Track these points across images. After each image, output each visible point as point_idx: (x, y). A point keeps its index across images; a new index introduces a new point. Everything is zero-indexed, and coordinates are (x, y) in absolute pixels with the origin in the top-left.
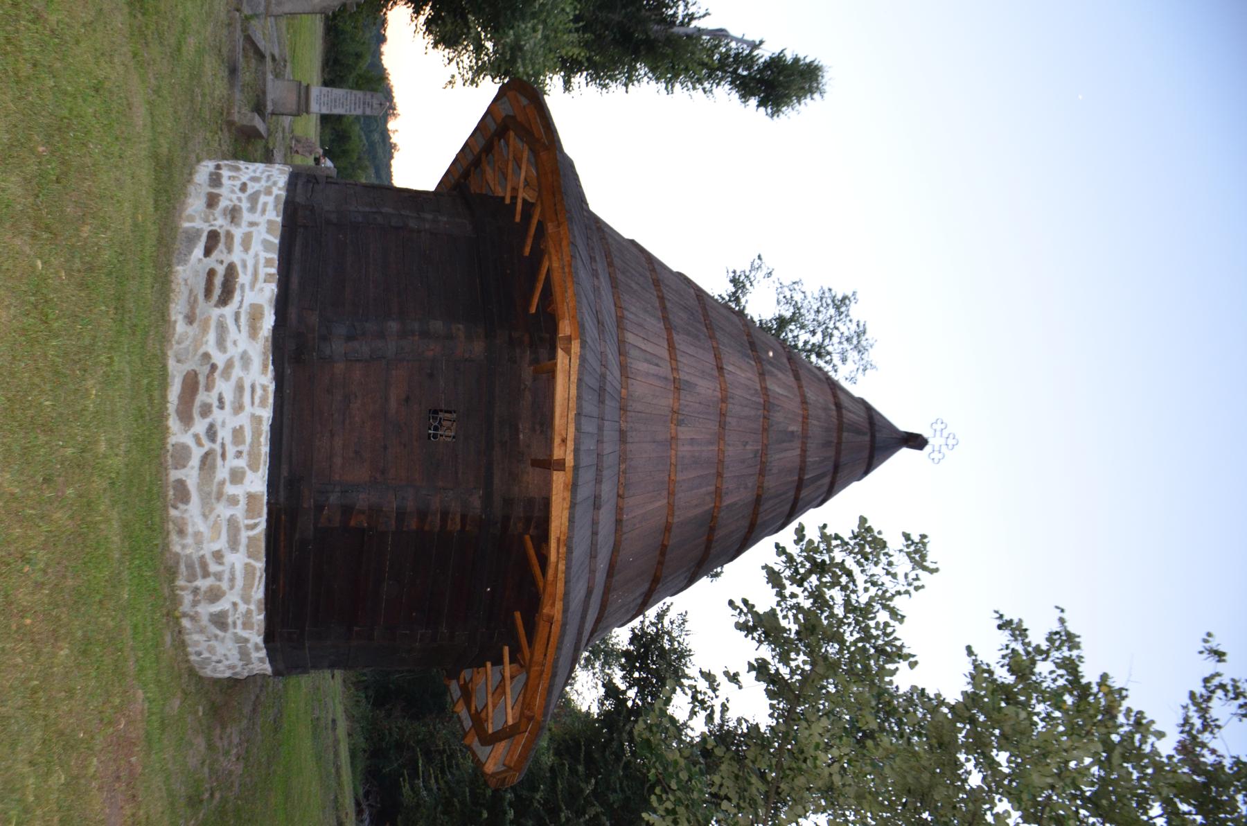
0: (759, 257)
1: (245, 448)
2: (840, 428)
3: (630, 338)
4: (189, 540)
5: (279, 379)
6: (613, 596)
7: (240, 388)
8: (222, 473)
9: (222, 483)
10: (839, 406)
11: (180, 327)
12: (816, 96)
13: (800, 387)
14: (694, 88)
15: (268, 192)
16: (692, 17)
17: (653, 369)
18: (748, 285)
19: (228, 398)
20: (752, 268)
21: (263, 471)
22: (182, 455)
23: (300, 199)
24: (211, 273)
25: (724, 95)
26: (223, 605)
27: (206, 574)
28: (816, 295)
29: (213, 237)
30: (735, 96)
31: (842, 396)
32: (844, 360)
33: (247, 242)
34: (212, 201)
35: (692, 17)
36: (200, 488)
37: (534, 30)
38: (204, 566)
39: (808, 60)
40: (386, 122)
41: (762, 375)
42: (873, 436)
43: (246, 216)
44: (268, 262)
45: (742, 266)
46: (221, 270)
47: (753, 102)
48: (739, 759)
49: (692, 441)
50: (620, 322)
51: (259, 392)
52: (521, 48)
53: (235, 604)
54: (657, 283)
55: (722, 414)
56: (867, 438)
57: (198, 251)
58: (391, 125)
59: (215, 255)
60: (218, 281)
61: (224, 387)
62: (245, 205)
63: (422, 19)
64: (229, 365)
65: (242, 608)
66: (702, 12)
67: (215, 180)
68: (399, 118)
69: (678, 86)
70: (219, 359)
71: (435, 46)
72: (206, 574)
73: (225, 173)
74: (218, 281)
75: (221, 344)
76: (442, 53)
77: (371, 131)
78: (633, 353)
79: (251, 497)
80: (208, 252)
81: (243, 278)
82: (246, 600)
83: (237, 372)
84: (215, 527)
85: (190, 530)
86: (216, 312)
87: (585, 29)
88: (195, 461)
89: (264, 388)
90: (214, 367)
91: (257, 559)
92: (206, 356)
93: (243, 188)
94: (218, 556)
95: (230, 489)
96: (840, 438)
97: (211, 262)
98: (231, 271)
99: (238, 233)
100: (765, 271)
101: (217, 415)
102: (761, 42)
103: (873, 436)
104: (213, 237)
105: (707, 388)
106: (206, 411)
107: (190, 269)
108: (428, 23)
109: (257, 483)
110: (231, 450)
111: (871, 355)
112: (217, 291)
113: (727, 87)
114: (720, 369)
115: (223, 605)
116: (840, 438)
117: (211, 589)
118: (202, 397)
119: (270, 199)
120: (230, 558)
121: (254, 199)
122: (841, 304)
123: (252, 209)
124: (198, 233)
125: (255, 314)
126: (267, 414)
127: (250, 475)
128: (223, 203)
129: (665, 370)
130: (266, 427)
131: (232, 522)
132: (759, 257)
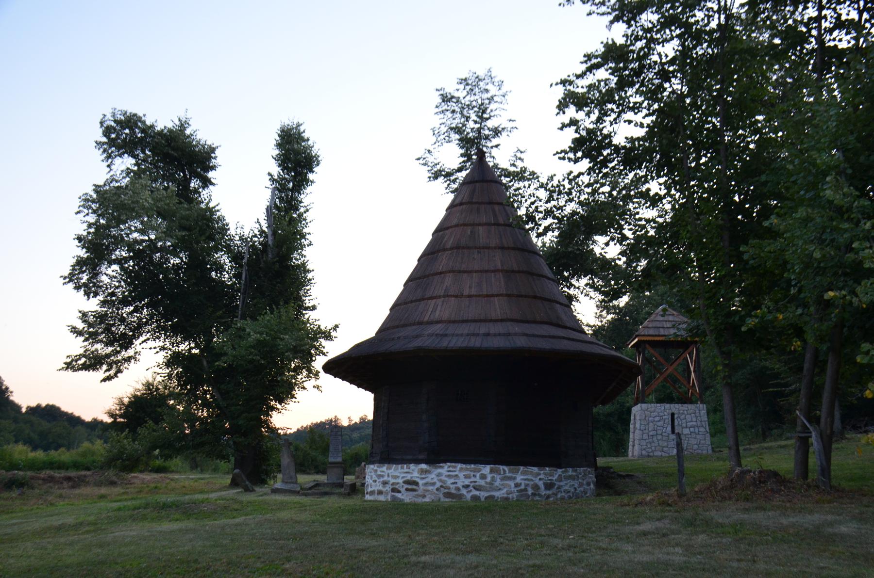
0: (418, 159)
1: (472, 474)
2: (470, 203)
3: (426, 319)
4: (510, 496)
5: (445, 462)
6: (538, 319)
7: (449, 476)
8: (482, 483)
9: (486, 483)
10: (461, 204)
11: (427, 500)
12: (302, 129)
13: (451, 227)
14: (305, 220)
15: (376, 471)
16: (262, 232)
17: (439, 308)
18: (438, 167)
19: (452, 481)
20: (425, 164)
21: (481, 466)
22: (475, 498)
23: (378, 458)
24: (407, 490)
25: (309, 197)
26: (541, 484)
27: (525, 490)
28: (442, 116)
29: (393, 490)
30: (309, 189)
31: (457, 201)
32: (487, 91)
33: (396, 477)
34: (380, 493)
35: (262, 232)
36: (489, 491)
37: (282, 340)
38: (521, 491)
39: (278, 138)
40: (343, 427)
41: (445, 250)
42: (477, 182)
43: (386, 478)
44: (402, 468)
45: (425, 173)
46: (406, 486)
47: (311, 176)
48: (679, 220)
49: (470, 287)
50: (420, 323)
51: (451, 469)
52: (295, 347)
53: (540, 479)
54: (433, 253)
55: (460, 272)
56: (478, 185)
57: (399, 495)
58: (345, 423)
59: (400, 489)
60: (410, 487)
61: (449, 482)
62: (382, 480)
63: (279, 406)
64: (441, 481)
65: (542, 476)
66: (257, 226)
67: (372, 493)
68: (339, 417)
69: (305, 230)
70: (438, 484)
71: (293, 397)
72: (525, 490)
73: (370, 489)
74: (410, 487)
75: (433, 484)
76: (298, 393)
77: (351, 440)
78: (432, 318)
79: (491, 471)
80: (399, 492)
81: (409, 477)
82: (539, 474)
83: (443, 478)
84: (504, 486)
85: (505, 495)
86: (421, 487)
87: (277, 305)
88: (477, 493)
89: (449, 467)
90: (441, 486)
91: (519, 470)
92: (437, 489)
93: (375, 481)
94: (517, 485)
95: (489, 479)
96: (476, 203)
97: (403, 490)
98: (407, 482)
99: (392, 481)
100: (427, 155)
101: (460, 485)
102: (269, 174)
103: (477, 182)
104: (393, 490)
105: (449, 280)
106: (458, 489)
107: (406, 497)
108: (281, 402)
109: (486, 469)
110: (473, 479)
111: (482, 73)
112: (414, 487)
113: (302, 196)
114: (441, 273)
115: (541, 484)
116: (476, 203)
117: (533, 488)
118: (453, 491)
119: (379, 470)
120: (518, 480)
121: (380, 476)
122: (446, 99)
123: (382, 476)
124: (393, 496)
125: (422, 471)
126: (459, 466)
127: (483, 472)
128: (381, 488)
129: (440, 301)
130: (464, 466)
131: (502, 479)
132: (418, 159)
